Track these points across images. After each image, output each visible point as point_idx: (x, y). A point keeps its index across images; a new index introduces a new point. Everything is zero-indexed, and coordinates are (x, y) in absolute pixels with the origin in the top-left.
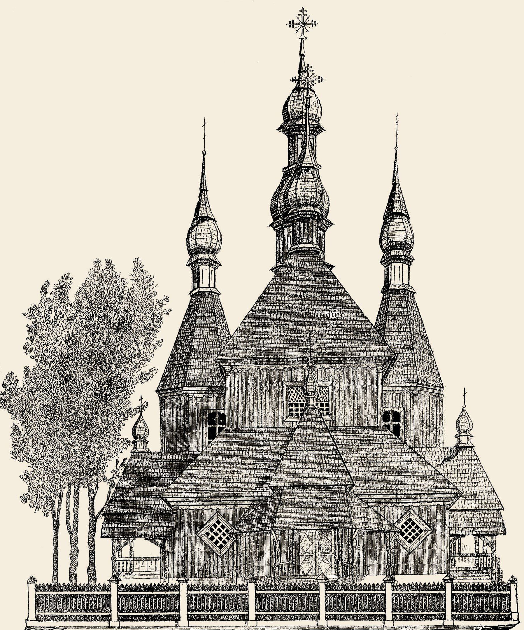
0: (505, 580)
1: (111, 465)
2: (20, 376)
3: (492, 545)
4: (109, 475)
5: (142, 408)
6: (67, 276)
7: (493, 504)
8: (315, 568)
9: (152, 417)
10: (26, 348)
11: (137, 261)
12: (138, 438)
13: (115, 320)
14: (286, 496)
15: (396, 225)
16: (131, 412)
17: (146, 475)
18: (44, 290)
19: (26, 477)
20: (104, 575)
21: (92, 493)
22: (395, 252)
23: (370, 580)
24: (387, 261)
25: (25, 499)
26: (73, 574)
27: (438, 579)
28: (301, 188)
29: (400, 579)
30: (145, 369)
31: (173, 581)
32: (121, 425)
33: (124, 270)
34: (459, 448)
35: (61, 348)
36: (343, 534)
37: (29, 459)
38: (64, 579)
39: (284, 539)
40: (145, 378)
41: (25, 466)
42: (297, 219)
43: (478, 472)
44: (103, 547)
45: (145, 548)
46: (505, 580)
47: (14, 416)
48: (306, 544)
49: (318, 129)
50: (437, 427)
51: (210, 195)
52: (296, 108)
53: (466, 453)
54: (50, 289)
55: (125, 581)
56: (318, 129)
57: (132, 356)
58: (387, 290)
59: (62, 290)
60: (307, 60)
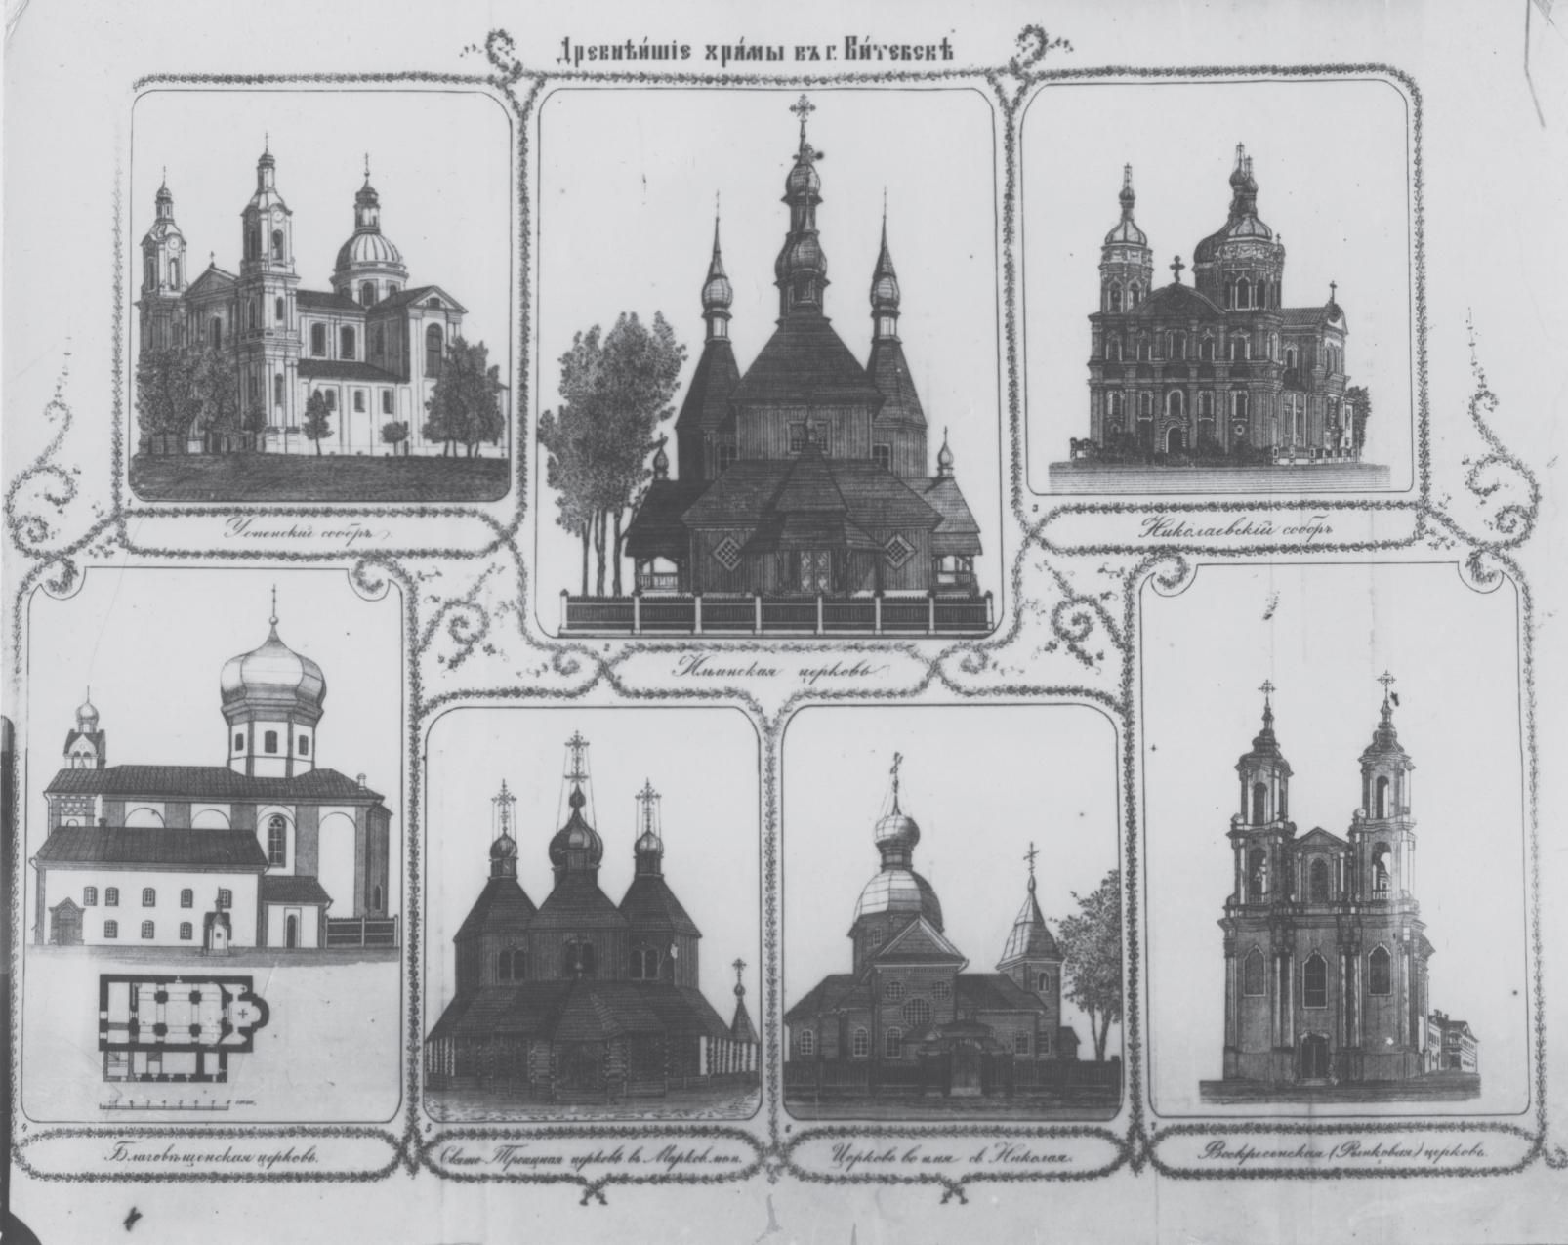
0: (982, 593)
1: (634, 493)
2: (555, 413)
3: (971, 563)
4: (632, 501)
5: (663, 442)
6: (597, 328)
7: (972, 529)
8: (814, 583)
9: (671, 450)
10: (562, 391)
11: (658, 314)
12: (661, 467)
13: (638, 363)
14: (790, 520)
15: (885, 284)
16: (652, 446)
17: (662, 498)
18: (576, 339)
19: (560, 502)
20: (628, 587)
21: (618, 517)
22: (885, 307)
23: (863, 594)
24: (876, 315)
25: (559, 522)
26: (600, 586)
27: (922, 593)
28: (801, 252)
29: (889, 594)
30: (666, 407)
31: (689, 595)
32: (643, 457)
33: (647, 322)
34: (940, 480)
35: (592, 390)
36: (839, 556)
37: (563, 487)
38: (592, 591)
39: (786, 556)
40: (666, 415)
41: (560, 493)
42: (800, 275)
43: (959, 502)
44: (628, 564)
45: (663, 565)
46: (982, 593)
47: (550, 449)
48: (805, 562)
49: (817, 200)
50: (921, 459)
51: (724, 256)
52: (798, 181)
53: (947, 484)
54: (582, 338)
55: (647, 594)
56: (817, 200)
57: (654, 397)
58: (877, 341)
59: (592, 338)
60: (807, 140)
